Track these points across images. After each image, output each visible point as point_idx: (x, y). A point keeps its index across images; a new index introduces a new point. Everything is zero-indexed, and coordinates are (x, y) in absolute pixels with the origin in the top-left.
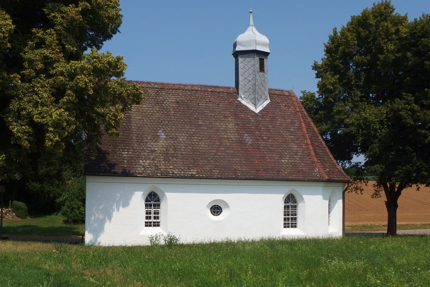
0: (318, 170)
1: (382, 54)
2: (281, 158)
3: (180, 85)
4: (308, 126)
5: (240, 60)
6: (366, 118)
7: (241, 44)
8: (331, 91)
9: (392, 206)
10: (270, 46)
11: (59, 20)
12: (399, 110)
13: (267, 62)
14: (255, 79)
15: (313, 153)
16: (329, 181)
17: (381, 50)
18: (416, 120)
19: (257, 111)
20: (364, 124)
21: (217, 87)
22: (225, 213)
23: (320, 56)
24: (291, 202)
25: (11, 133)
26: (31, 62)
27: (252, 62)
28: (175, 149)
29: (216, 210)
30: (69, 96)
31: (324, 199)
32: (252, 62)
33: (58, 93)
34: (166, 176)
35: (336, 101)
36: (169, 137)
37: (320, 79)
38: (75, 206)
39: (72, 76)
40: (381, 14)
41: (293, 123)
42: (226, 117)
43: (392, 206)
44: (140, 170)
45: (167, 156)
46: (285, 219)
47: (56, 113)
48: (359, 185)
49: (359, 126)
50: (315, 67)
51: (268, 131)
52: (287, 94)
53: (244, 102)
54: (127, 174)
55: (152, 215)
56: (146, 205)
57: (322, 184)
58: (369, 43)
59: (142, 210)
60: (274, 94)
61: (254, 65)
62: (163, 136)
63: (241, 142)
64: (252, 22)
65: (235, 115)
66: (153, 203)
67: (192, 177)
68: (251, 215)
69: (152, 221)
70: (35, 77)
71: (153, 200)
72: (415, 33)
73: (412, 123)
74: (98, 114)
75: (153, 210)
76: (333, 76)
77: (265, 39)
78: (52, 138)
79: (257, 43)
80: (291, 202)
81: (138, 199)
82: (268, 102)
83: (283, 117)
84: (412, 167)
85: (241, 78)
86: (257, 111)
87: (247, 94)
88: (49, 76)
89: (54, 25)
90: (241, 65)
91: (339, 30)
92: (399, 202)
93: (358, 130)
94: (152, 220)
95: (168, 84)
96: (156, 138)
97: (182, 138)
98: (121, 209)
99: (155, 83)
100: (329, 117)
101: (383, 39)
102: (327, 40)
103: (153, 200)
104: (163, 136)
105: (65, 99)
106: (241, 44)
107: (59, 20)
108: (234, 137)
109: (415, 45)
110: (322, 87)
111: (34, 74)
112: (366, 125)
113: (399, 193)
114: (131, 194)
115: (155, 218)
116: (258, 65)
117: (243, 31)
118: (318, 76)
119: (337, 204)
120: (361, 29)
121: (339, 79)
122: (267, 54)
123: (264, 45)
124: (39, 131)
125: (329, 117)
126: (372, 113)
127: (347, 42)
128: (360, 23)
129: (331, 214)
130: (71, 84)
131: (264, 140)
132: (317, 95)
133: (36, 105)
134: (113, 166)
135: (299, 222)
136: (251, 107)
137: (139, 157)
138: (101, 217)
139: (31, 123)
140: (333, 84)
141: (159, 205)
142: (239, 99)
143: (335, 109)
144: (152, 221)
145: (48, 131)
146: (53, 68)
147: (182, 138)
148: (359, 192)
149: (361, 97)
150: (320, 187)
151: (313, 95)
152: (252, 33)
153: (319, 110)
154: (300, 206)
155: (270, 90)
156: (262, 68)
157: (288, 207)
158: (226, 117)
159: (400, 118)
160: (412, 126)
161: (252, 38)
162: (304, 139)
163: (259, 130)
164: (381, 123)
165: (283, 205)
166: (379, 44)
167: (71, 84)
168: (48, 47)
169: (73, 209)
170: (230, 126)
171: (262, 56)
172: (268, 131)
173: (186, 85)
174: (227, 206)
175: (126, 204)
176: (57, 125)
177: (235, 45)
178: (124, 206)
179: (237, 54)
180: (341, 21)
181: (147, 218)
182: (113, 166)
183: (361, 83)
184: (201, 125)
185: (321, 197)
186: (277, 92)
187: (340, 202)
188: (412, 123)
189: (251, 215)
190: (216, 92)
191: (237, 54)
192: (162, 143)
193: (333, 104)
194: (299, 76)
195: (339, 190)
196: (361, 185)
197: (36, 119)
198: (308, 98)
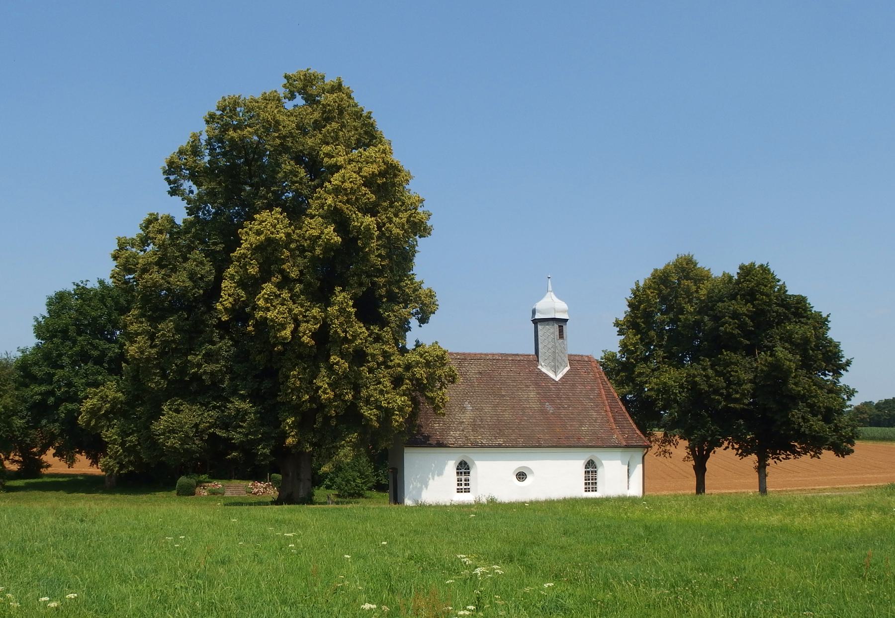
0: (616, 437)
1: (683, 314)
2: (581, 426)
3: (481, 354)
4: (608, 392)
5: (540, 327)
6: (665, 383)
7: (539, 312)
8: (633, 352)
9: (700, 470)
10: (568, 312)
11: (393, 318)
12: (694, 376)
13: (567, 328)
14: (555, 347)
15: (612, 421)
16: (627, 447)
17: (681, 311)
18: (710, 386)
19: (557, 379)
20: (664, 388)
21: (517, 355)
22: (529, 480)
23: (621, 311)
24: (591, 467)
25: (362, 415)
26: (373, 356)
27: (552, 330)
28: (481, 420)
29: (521, 476)
30: (407, 385)
31: (623, 463)
32: (552, 330)
33: (397, 381)
34: (475, 445)
35: (637, 362)
36: (475, 409)
37: (622, 337)
38: (350, 478)
39: (408, 367)
40: (683, 270)
41: (592, 390)
42: (527, 386)
43: (700, 470)
44: (452, 441)
45: (475, 427)
46: (586, 484)
47: (400, 400)
48: (668, 448)
49: (658, 390)
50: (617, 324)
51: (569, 399)
52: (586, 359)
53: (544, 370)
54: (440, 445)
55: (463, 482)
56: (458, 473)
57: (620, 450)
58: (671, 300)
59: (455, 477)
60: (574, 360)
61: (553, 333)
62: (469, 407)
63: (543, 412)
64: (550, 289)
65: (537, 384)
66: (463, 471)
67: (500, 446)
68: (555, 477)
69: (463, 487)
70: (377, 369)
71: (464, 468)
72: (712, 297)
73: (707, 389)
74: (427, 397)
75: (463, 477)
76: (635, 335)
77: (563, 305)
78: (398, 419)
79: (556, 311)
80: (591, 467)
81: (451, 467)
82: (568, 368)
83: (583, 385)
84: (708, 431)
85: (540, 346)
86: (557, 379)
87: (547, 361)
88: (388, 367)
89: (389, 323)
90: (540, 333)
91: (641, 284)
92: (708, 465)
93: (657, 395)
94: (463, 487)
95: (469, 354)
96: (463, 409)
97: (488, 409)
98: (436, 477)
99: (458, 354)
100: (630, 379)
101: (684, 298)
102: (629, 295)
103: (464, 468)
104: (469, 407)
105: (404, 387)
106: (539, 312)
107: (393, 318)
108: (535, 406)
109: (712, 309)
110: (624, 346)
111: (376, 366)
112: (665, 390)
113: (707, 456)
114: (445, 464)
115: (466, 485)
116: (558, 333)
117: (542, 297)
118: (621, 333)
119: (447, 468)
120: (662, 287)
121: (640, 339)
122: (566, 320)
123: (563, 311)
124: (388, 413)
125: (630, 379)
126: (671, 376)
127: (648, 301)
128: (661, 279)
129: (631, 479)
130: (409, 374)
131: (565, 408)
132: (619, 355)
133: (381, 392)
134: (428, 438)
135: (599, 486)
136: (551, 375)
137: (449, 428)
138: (419, 485)
139: (379, 408)
140: (634, 345)
141: (469, 473)
142: (539, 367)
143: (637, 370)
144: (463, 487)
145: (393, 414)
146: (391, 361)
147: (488, 409)
148: (667, 455)
149: (664, 358)
150: (618, 453)
151: (614, 355)
152: (550, 300)
153: (620, 370)
154: (600, 471)
155: (570, 356)
156: (561, 336)
157: (588, 472)
158: (527, 386)
159: (695, 384)
160: (706, 391)
161: (551, 305)
162: (603, 402)
163: (560, 398)
164: (681, 386)
165: (584, 470)
166: (680, 304)
167: (409, 374)
168: (384, 343)
169: (348, 481)
170: (532, 395)
171: (561, 323)
172: (569, 399)
173: (486, 355)
174: (532, 472)
175: (440, 474)
176: (401, 409)
177: (534, 312)
178: (438, 476)
179: (536, 322)
180: (643, 275)
181: (458, 485)
182: (428, 438)
183: (664, 343)
184: (504, 396)
185: (619, 462)
186: (577, 358)
187: (640, 467)
188: (707, 389)
189: (555, 477)
190: (516, 360)
191: (536, 322)
192: (468, 416)
193: (635, 366)
194: (599, 336)
195: (638, 455)
196: (671, 448)
197: (384, 404)
198: (610, 357)
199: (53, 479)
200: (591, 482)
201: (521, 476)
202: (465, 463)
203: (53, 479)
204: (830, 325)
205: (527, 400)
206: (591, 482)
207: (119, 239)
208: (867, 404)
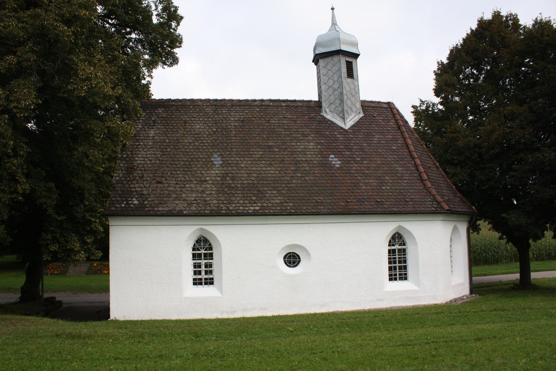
41: (394, 140)
53: (329, 116)
54: (452, 233)
55: (203, 268)
56: (194, 255)
63: (326, 165)
86: (347, 127)
87: (333, 106)
94: (203, 276)
144: (204, 276)
156: (351, 73)
157: (394, 251)
158: (305, 135)
163: (350, 150)
165: (387, 248)
174: (308, 254)
199: (40, 289)
200: (398, 268)
201: (292, 259)
202: (206, 241)
203: (40, 289)
204: (469, 32)
205: (304, 152)
206: (398, 268)
207: (182, 18)
208: (155, 99)
